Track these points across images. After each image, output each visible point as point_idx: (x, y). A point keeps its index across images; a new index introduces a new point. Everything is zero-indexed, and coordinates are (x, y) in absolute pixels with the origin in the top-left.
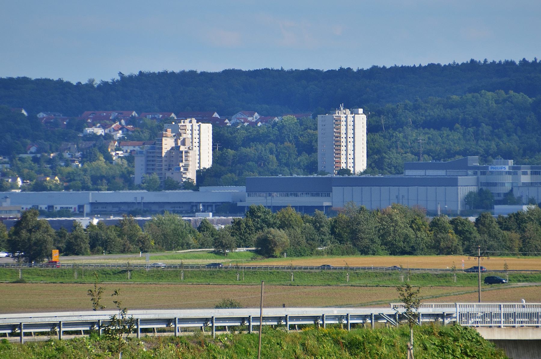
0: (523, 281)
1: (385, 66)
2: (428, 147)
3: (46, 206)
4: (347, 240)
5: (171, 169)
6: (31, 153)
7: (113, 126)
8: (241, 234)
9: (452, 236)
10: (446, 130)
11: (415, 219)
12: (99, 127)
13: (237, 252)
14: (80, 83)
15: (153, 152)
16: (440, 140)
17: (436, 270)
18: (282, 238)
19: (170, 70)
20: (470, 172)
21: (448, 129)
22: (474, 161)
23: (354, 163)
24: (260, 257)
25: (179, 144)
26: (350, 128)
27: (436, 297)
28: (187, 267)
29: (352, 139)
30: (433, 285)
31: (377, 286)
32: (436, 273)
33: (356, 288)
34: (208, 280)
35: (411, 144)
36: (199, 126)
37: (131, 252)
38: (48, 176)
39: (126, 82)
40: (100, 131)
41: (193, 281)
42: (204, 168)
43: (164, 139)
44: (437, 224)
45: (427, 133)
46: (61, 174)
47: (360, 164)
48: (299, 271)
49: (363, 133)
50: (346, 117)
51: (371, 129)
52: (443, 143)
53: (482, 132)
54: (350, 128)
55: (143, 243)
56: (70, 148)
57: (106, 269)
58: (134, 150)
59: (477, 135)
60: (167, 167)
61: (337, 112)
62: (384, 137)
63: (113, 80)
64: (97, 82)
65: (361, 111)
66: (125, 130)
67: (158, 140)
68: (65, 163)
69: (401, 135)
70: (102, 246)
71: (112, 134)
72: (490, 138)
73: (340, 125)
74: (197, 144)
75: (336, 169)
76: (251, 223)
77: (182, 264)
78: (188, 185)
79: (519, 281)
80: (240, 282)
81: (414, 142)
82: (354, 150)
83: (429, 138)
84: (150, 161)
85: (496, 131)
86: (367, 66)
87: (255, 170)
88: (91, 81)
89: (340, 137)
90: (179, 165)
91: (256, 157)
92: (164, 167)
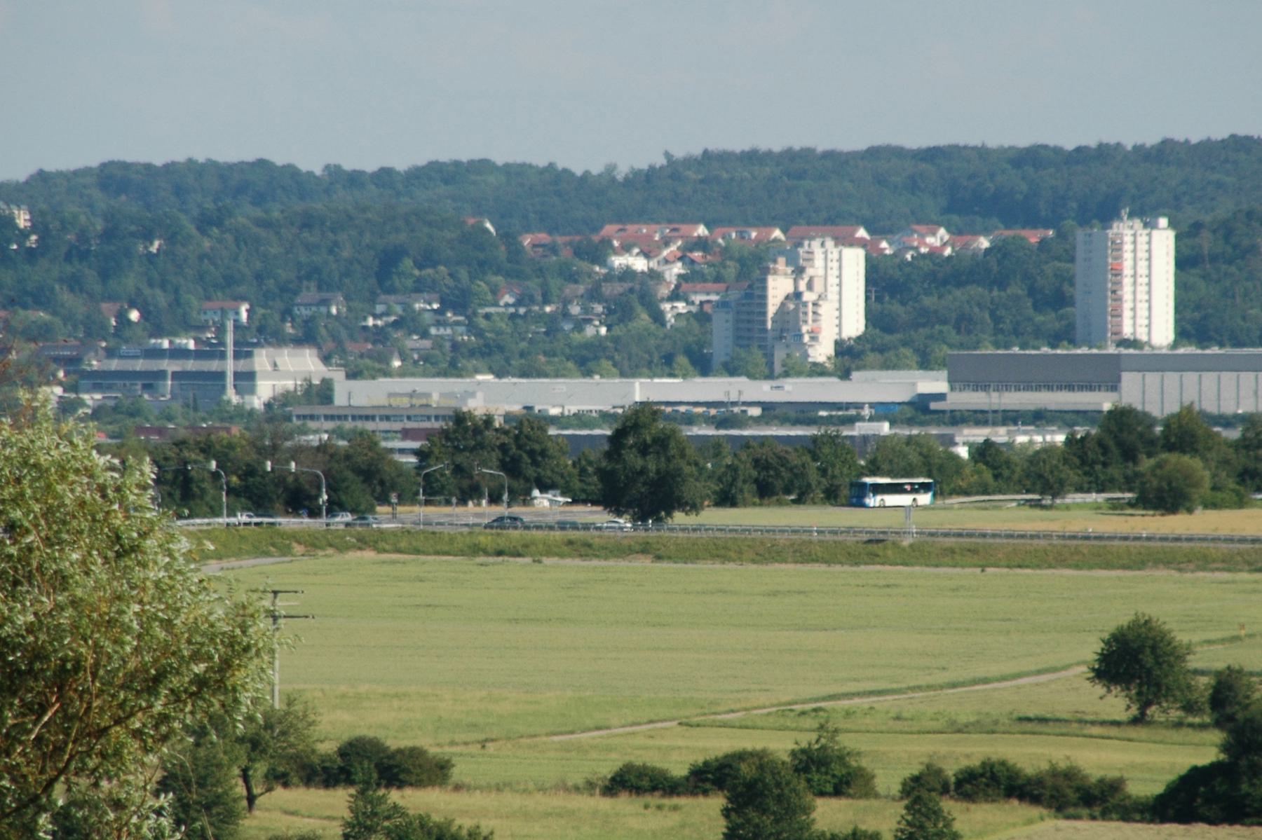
12: (638, 254)
29: (1145, 277)
36: (840, 253)
40: (640, 264)
50: (1134, 235)
51: (1182, 263)
57: (782, 539)
58: (708, 302)
62: (1204, 277)
64: (622, 172)
65: (1163, 222)
74: (832, 289)
78: (818, 370)
88: (611, 169)
90: (800, 330)
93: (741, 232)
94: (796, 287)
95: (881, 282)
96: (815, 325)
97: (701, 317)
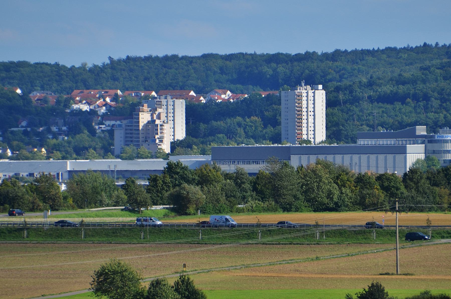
0: (447, 237)
1: (347, 49)
2: (382, 120)
3: (27, 173)
4: (269, 197)
5: (147, 141)
6: (22, 127)
7: (98, 103)
8: (157, 191)
9: (378, 191)
10: (398, 104)
11: (340, 175)
12: (85, 104)
13: (153, 210)
14: (74, 66)
15: (131, 126)
16: (393, 113)
17: (355, 226)
18: (196, 194)
19: (154, 55)
20: (420, 140)
21: (400, 103)
22: (421, 130)
23: (314, 134)
24: (173, 214)
25: (155, 118)
26: (311, 102)
27: (352, 255)
28: (88, 225)
29: (313, 111)
30: (350, 242)
31: (290, 244)
32: (354, 229)
33: (268, 246)
34: (110, 239)
35: (366, 117)
36: (174, 102)
37: (41, 210)
38: (36, 148)
39: (114, 65)
40: (85, 108)
41: (95, 239)
42: (178, 140)
43: (140, 113)
44: (362, 180)
45: (381, 107)
46: (48, 146)
47: (321, 136)
48: (208, 228)
49: (322, 108)
51: (330, 104)
52: (396, 116)
53: (431, 106)
54: (311, 102)
55: (54, 200)
56: (57, 123)
59: (426, 109)
60: (144, 139)
61: (298, 88)
62: (342, 111)
63: (104, 64)
64: (90, 65)
65: (320, 87)
66: (108, 106)
67: (136, 114)
68: (53, 136)
69: (356, 110)
70: (10, 204)
71: (97, 110)
72: (439, 111)
73: (302, 100)
75: (298, 140)
76: (168, 180)
77: (82, 221)
79: (443, 237)
80: (145, 240)
81: (369, 115)
82: (314, 123)
83: (383, 112)
84: (128, 133)
85: (444, 104)
86: (330, 50)
87: (223, 142)
88: (84, 65)
89: (302, 111)
90: (155, 137)
91: (226, 130)
92: (141, 139)
93: (137, 93)
94: (152, 117)
95: (193, 115)
96: (162, 135)
97: (111, 132)
